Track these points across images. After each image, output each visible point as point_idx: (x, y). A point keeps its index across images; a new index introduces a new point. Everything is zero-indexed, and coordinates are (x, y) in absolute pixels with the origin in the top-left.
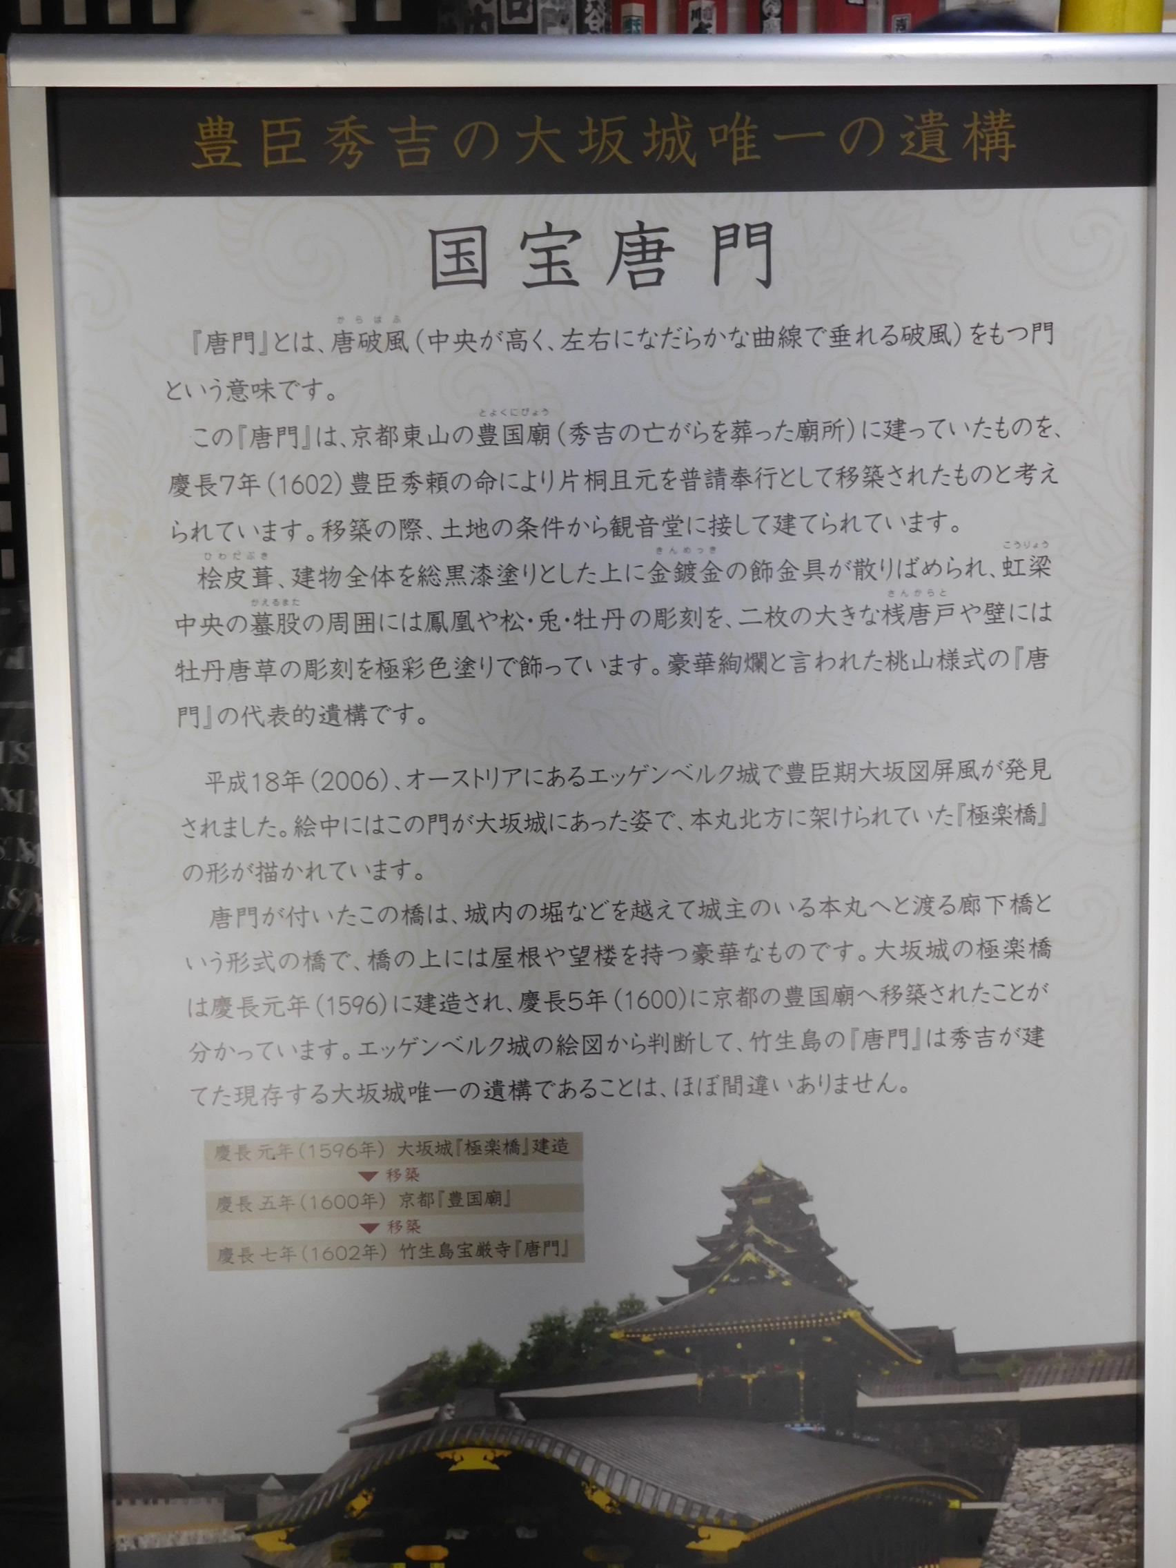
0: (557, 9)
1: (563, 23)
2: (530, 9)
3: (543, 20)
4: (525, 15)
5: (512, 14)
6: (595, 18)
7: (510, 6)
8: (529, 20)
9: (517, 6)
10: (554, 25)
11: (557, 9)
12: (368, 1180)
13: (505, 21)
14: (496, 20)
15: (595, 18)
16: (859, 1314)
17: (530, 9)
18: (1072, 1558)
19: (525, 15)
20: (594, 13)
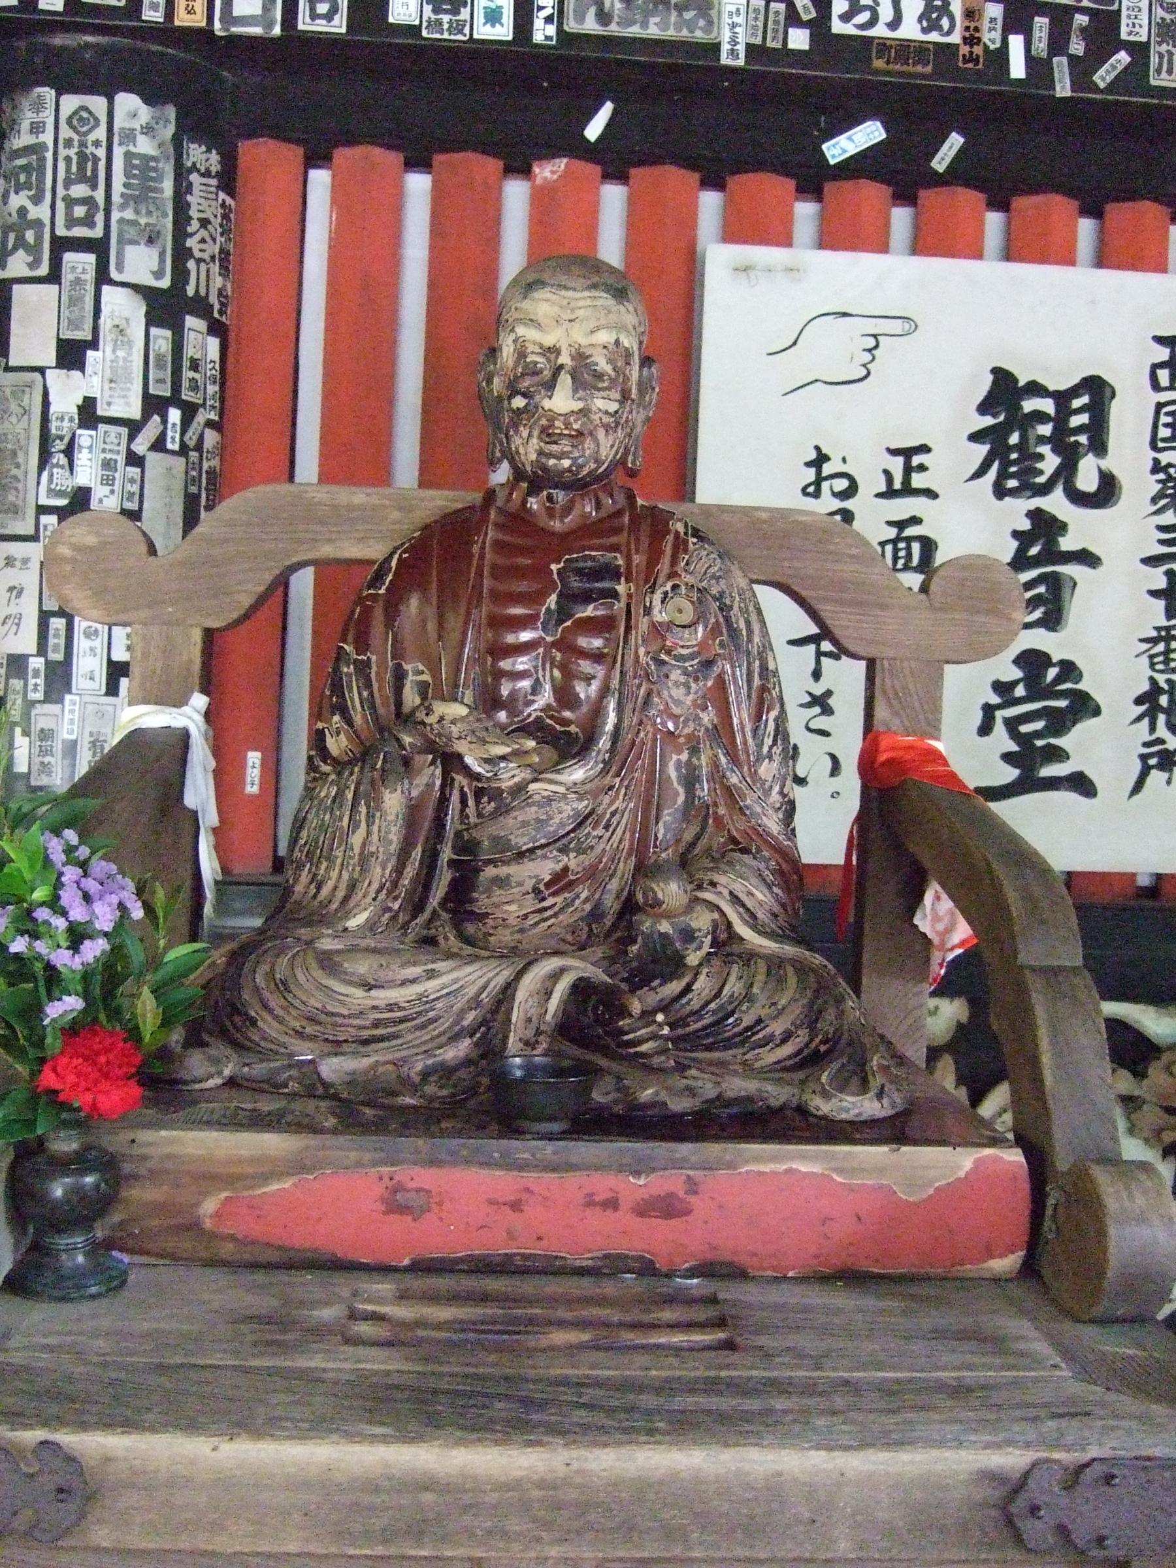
0: (143, 221)
1: (150, 241)
2: (99, 218)
3: (120, 235)
4: (91, 225)
5: (71, 222)
6: (203, 241)
7: (312, 9)
8: (98, 232)
9: (322, 8)
10: (137, 243)
11: (143, 221)
12: (929, 1048)
13: (61, 231)
14: (47, 230)
15: (203, 241)
16: (875, 1395)
17: (99, 218)
18: (47, 1537)
19: (91, 225)
20: (203, 233)
